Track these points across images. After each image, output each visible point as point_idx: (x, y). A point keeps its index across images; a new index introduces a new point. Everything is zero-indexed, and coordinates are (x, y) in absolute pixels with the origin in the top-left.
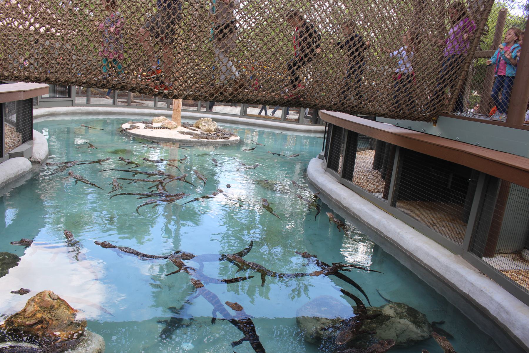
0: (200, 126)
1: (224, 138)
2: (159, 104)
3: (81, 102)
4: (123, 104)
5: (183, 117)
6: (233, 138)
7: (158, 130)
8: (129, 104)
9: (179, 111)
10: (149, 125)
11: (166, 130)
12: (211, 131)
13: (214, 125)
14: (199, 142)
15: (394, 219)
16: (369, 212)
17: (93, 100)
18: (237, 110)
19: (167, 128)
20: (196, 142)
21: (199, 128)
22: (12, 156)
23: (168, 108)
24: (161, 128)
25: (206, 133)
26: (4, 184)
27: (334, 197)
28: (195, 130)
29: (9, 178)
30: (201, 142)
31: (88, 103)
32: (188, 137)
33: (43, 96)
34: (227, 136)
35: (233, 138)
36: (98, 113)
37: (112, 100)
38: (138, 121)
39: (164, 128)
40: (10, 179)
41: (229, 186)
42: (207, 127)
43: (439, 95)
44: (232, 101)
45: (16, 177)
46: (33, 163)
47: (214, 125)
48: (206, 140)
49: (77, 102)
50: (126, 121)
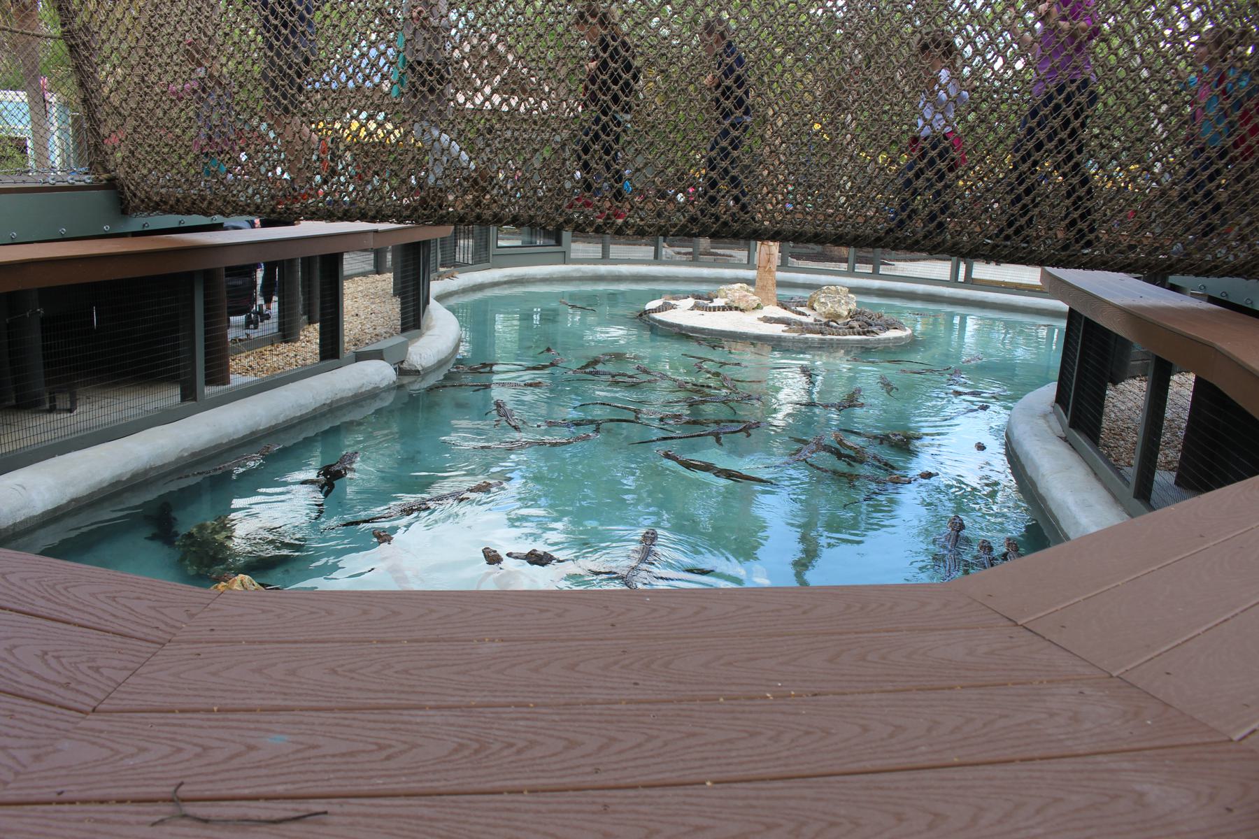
0: (815, 305)
1: (864, 334)
2: (667, 251)
3: (591, 256)
4: (684, 258)
5: (781, 284)
6: (892, 334)
7: (717, 313)
8: (694, 260)
9: (770, 271)
10: (703, 301)
11: (734, 312)
12: (839, 316)
13: (847, 303)
14: (799, 341)
15: (74, 496)
16: (1073, 508)
17: (616, 250)
18: (940, 269)
19: (736, 309)
20: (794, 340)
21: (814, 309)
22: (360, 357)
23: (750, 265)
24: (724, 309)
25: (825, 320)
26: (326, 408)
27: (1029, 473)
28: (804, 314)
29: (338, 397)
30: (806, 341)
31: (605, 258)
32: (777, 330)
33: (501, 243)
34: (874, 329)
35: (892, 334)
36: (619, 278)
37: (746, 253)
38: (676, 295)
39: (731, 309)
40: (342, 399)
41: (981, 447)
42: (830, 307)
43: (1023, 191)
44: (932, 247)
45: (355, 395)
46: (401, 372)
47: (847, 303)
48: (820, 336)
49: (573, 256)
50: (655, 295)
